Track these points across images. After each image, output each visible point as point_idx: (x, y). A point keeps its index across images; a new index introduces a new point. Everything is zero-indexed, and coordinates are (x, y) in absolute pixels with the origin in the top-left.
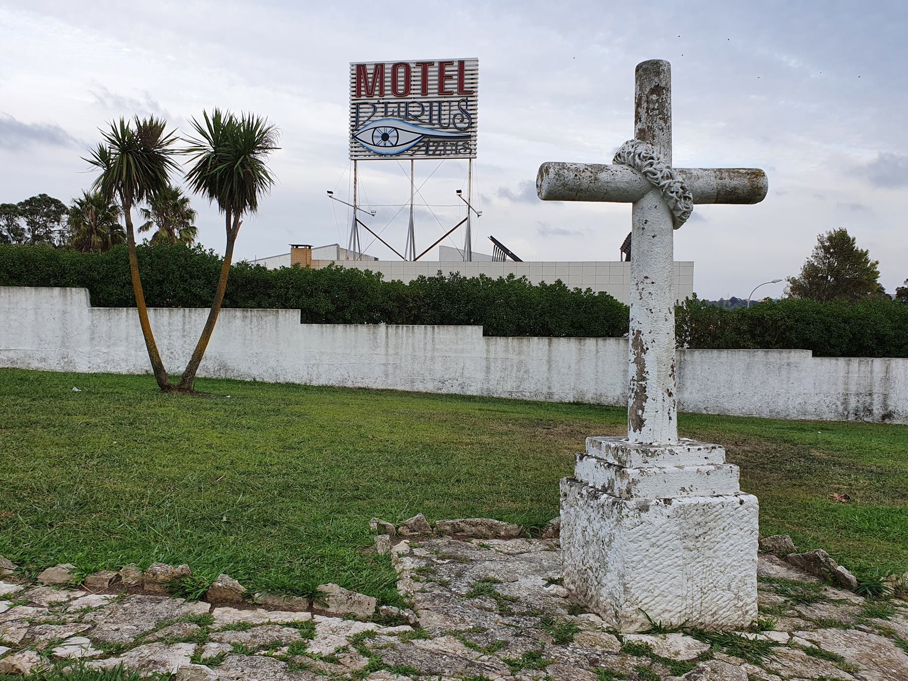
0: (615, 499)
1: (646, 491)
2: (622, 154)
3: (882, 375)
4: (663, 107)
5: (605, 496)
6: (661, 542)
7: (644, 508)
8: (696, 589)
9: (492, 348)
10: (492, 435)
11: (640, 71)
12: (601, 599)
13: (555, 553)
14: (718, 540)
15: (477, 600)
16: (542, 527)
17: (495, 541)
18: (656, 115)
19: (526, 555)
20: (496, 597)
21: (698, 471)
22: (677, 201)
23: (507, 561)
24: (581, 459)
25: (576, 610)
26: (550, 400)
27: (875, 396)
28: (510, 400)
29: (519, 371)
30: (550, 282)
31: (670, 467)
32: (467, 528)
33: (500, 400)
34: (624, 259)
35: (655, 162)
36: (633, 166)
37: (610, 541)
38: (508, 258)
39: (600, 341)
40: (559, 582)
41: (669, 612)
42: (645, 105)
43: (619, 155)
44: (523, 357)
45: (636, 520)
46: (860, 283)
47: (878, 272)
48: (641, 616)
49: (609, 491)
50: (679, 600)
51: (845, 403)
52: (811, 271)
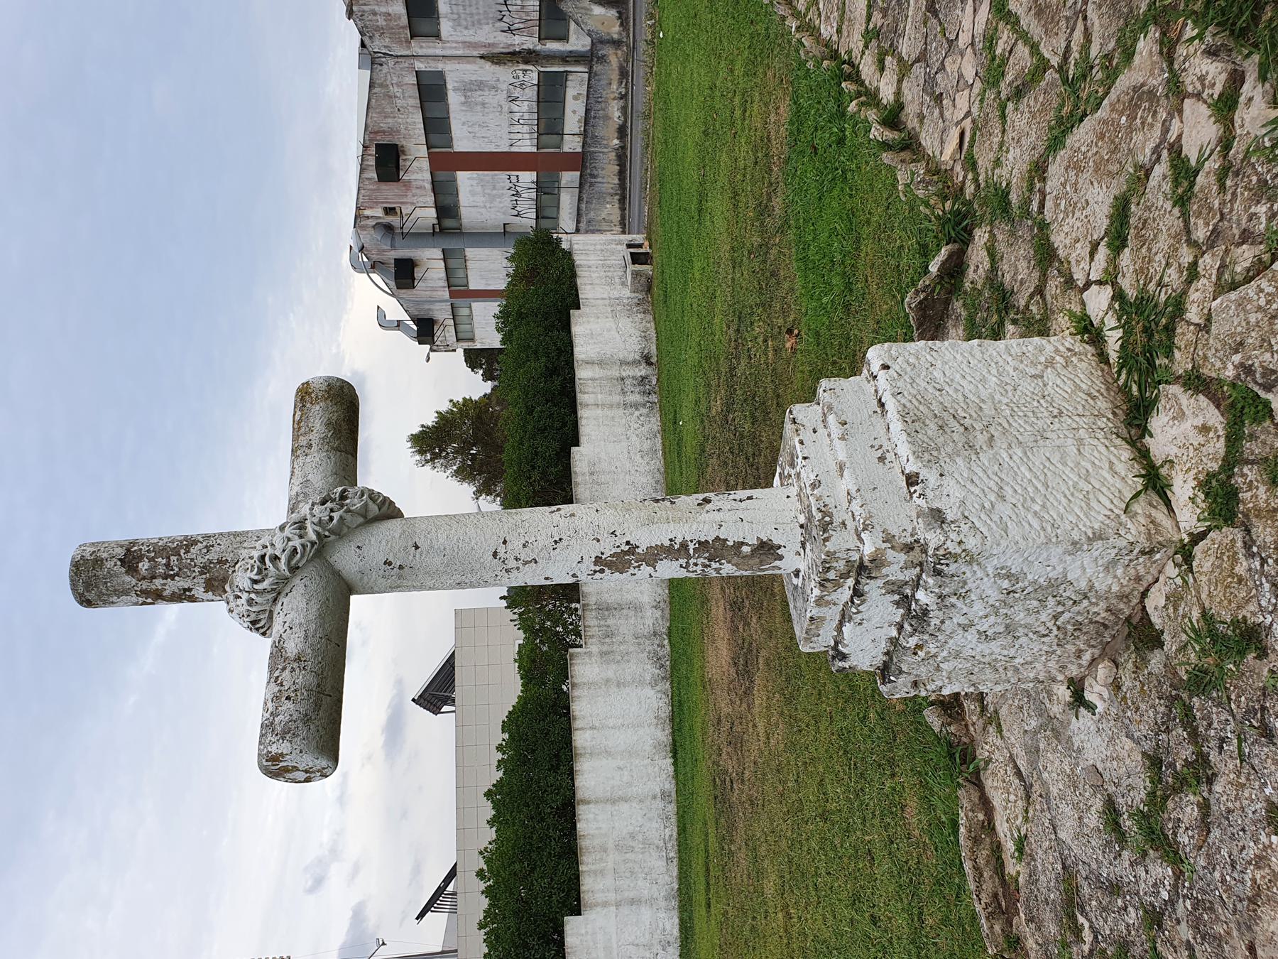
0: (926, 572)
1: (902, 517)
2: (253, 617)
3: (597, 368)
4: (165, 548)
5: (920, 595)
6: (992, 484)
7: (937, 517)
8: (1056, 426)
9: (600, 897)
10: (760, 874)
11: (91, 596)
12: (1115, 588)
13: (1003, 712)
14: (961, 398)
15: (1183, 838)
16: (950, 745)
17: (1002, 827)
18: (180, 560)
19: (1022, 764)
20: (1157, 801)
21: (842, 438)
22: (348, 511)
23: (1046, 797)
24: (844, 657)
25: (1143, 635)
26: (674, 794)
27: (624, 374)
28: (681, 860)
29: (632, 849)
30: (488, 811)
31: (847, 483)
32: (988, 887)
33: (684, 877)
34: (453, 708)
35: (269, 551)
36: (277, 593)
37: (1009, 576)
38: (450, 888)
39: (577, 724)
40: (1077, 689)
41: (1114, 469)
42: (158, 583)
43: (254, 623)
44: (611, 845)
45: (965, 528)
46: (479, 417)
47: (464, 399)
48: (1137, 508)
49: (908, 591)
50: (1086, 451)
51: (636, 406)
52: (464, 474)
